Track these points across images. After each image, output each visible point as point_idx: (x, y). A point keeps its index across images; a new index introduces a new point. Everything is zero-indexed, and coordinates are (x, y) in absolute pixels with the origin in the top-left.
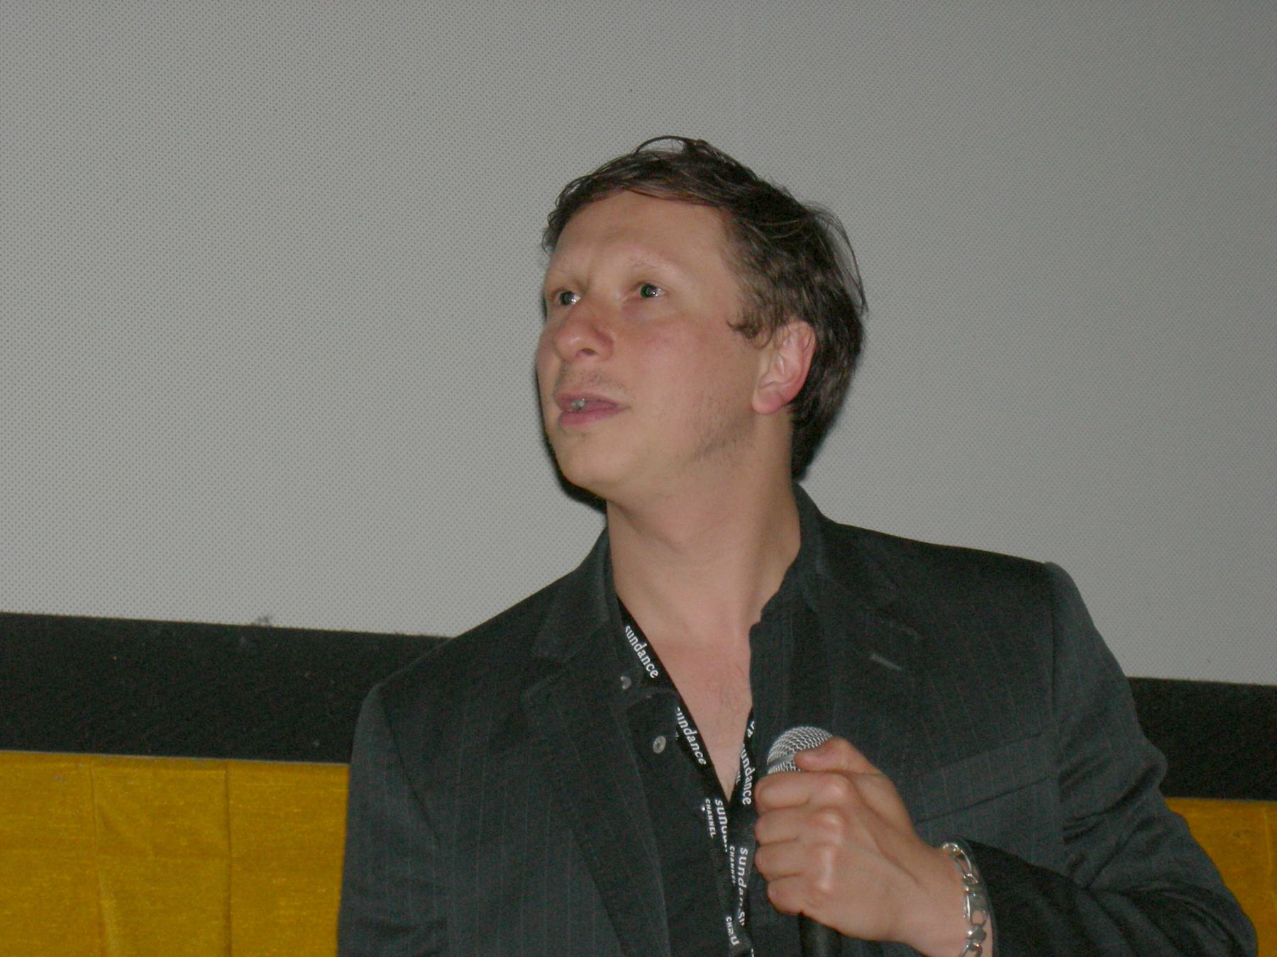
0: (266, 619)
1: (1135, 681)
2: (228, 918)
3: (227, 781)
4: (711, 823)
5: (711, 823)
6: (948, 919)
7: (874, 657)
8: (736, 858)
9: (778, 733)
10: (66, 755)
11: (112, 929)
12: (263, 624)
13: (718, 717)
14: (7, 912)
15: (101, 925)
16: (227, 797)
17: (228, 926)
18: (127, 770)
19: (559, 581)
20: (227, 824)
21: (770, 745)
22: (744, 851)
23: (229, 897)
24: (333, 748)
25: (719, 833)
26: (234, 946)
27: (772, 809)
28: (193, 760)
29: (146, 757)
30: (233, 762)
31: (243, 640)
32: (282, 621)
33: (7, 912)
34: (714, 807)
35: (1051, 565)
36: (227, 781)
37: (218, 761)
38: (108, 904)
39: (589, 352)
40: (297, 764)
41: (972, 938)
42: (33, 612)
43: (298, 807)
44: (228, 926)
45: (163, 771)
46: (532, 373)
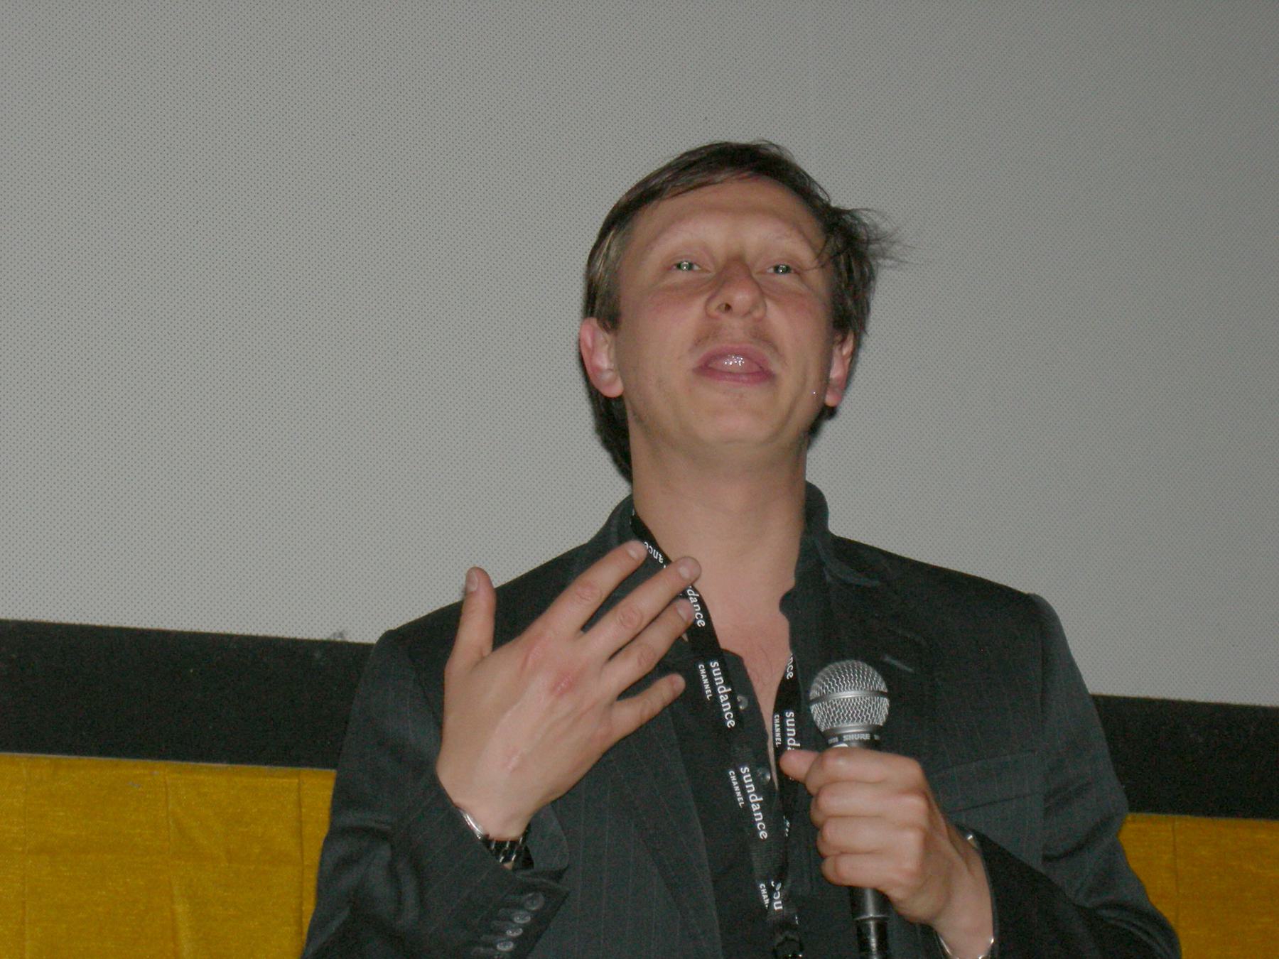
0: (341, 635)
1: (1095, 698)
3: (299, 789)
4: (739, 794)
5: (739, 794)
6: (970, 927)
7: (910, 670)
11: (185, 934)
12: (339, 639)
13: (1042, 870)
16: (299, 804)
19: (570, 553)
22: (744, 769)
24: (334, 766)
28: (265, 769)
30: (306, 771)
31: (317, 655)
34: (709, 670)
35: (1035, 596)
36: (299, 789)
38: (181, 908)
42: (112, 625)
46: (576, 346)
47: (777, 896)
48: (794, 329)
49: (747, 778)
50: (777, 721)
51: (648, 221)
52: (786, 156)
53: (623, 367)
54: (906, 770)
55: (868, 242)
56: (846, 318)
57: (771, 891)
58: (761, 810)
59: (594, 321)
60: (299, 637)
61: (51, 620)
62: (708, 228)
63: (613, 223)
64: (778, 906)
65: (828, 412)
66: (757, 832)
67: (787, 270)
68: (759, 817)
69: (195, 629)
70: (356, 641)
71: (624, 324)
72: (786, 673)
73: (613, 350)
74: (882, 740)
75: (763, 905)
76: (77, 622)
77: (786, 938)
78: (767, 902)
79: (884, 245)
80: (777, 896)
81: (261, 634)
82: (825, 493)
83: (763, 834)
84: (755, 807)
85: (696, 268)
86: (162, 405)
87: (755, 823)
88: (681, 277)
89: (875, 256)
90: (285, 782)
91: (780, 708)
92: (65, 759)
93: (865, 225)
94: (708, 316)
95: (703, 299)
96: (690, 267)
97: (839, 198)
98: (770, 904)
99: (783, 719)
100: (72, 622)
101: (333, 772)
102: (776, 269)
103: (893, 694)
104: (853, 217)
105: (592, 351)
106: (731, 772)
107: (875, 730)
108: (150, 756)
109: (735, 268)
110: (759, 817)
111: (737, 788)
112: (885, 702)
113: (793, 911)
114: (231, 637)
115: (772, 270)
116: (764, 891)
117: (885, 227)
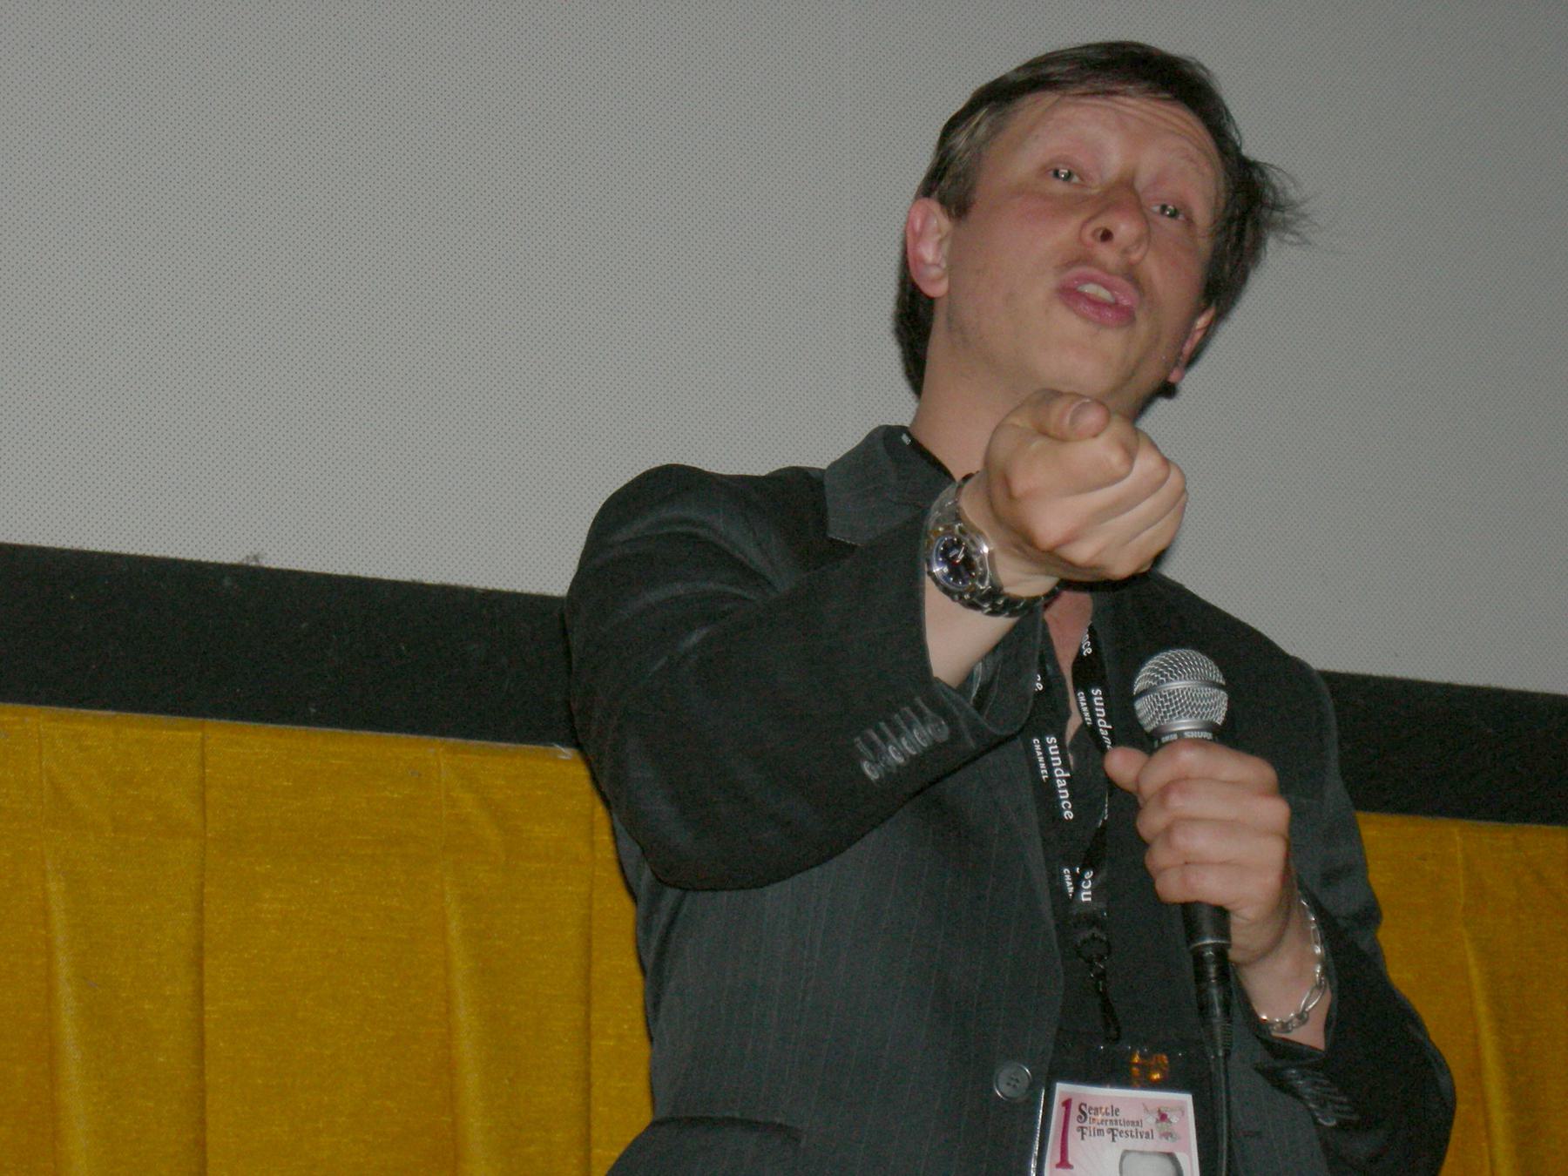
0: (256, 558)
2: (200, 910)
4: (1043, 766)
5: (1043, 766)
9: (1141, 662)
11: (59, 919)
12: (254, 564)
16: (203, 765)
17: (200, 922)
18: (82, 728)
20: (203, 797)
21: (1136, 672)
23: (202, 885)
25: (1052, 777)
27: (1137, 781)
31: (227, 582)
32: (278, 558)
38: (55, 886)
39: (964, 568)
44: (200, 922)
47: (1087, 886)
48: (1171, 280)
49: (1053, 750)
50: (1082, 699)
51: (1031, 107)
52: (1215, 85)
53: (955, 266)
54: (1250, 770)
55: (1276, 207)
56: (1220, 288)
57: (1077, 880)
58: (1068, 787)
59: (934, 206)
62: (1111, 136)
63: (989, 100)
64: (1085, 896)
65: (1167, 390)
66: (1062, 811)
67: (1174, 215)
68: (1064, 795)
71: (974, 214)
72: (1081, 651)
73: (946, 246)
74: (1227, 735)
75: (1067, 894)
77: (1093, 938)
78: (1071, 890)
79: (1288, 216)
80: (1087, 886)
83: (1068, 815)
84: (1061, 783)
85: (1076, 179)
87: (1060, 801)
88: (1058, 187)
89: (1272, 226)
93: (1274, 189)
94: (1080, 240)
95: (1083, 216)
96: (1069, 176)
97: (1252, 149)
102: (1164, 208)
103: (1231, 687)
104: (1262, 173)
105: (919, 236)
106: (1035, 740)
107: (1211, 727)
109: (1124, 193)
110: (1064, 795)
111: (1041, 759)
112: (1223, 696)
113: (1102, 905)
114: (119, 556)
115: (1157, 209)
116: (1068, 877)
117: (1293, 193)
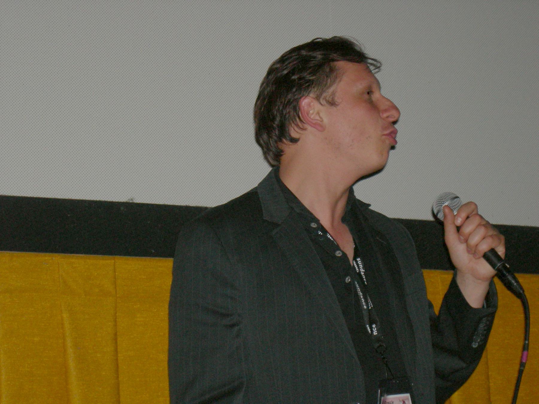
0: (132, 200)
2: (115, 321)
8: (358, 265)
10: (48, 254)
11: (67, 325)
14: (23, 319)
15: (63, 324)
16: (115, 272)
17: (116, 325)
18: (73, 260)
23: (116, 313)
26: (118, 333)
28: (100, 256)
29: (81, 255)
30: (117, 257)
31: (122, 208)
32: (139, 200)
33: (23, 319)
37: (111, 257)
38: (65, 315)
40: (144, 258)
41: (270, 137)
42: (35, 196)
43: (155, 274)
44: (116, 325)
45: (88, 261)
60: (114, 201)
61: (9, 195)
69: (70, 198)
70: (138, 202)
76: (20, 196)
81: (98, 200)
82: (339, 35)
86: (39, 98)
90: (108, 262)
91: (355, 259)
92: (16, 253)
98: (359, 270)
99: (357, 262)
100: (18, 195)
101: (171, 259)
108: (52, 251)
